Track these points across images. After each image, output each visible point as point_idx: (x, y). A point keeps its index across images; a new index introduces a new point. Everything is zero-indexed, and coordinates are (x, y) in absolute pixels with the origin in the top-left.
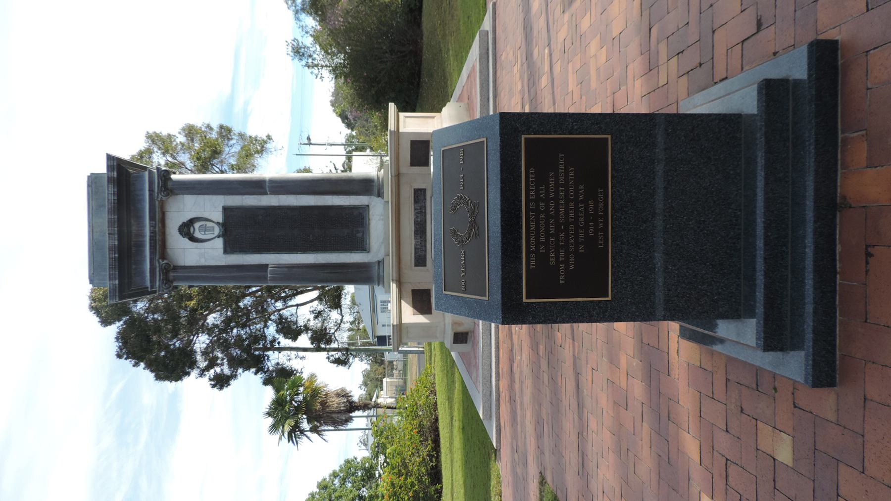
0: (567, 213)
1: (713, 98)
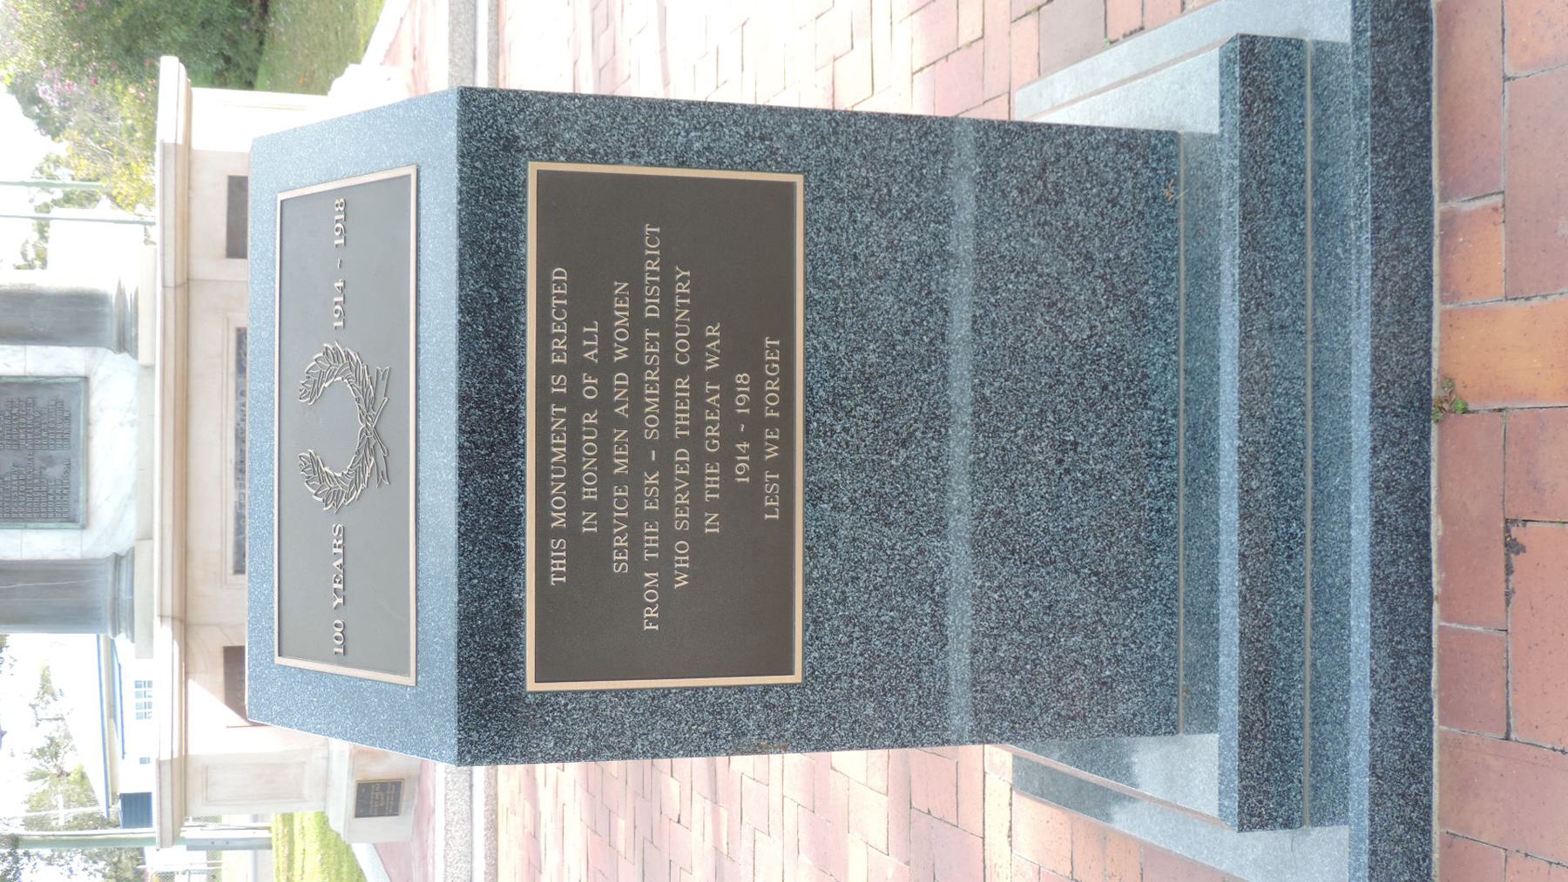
0: (666, 412)
1: (1104, 82)
